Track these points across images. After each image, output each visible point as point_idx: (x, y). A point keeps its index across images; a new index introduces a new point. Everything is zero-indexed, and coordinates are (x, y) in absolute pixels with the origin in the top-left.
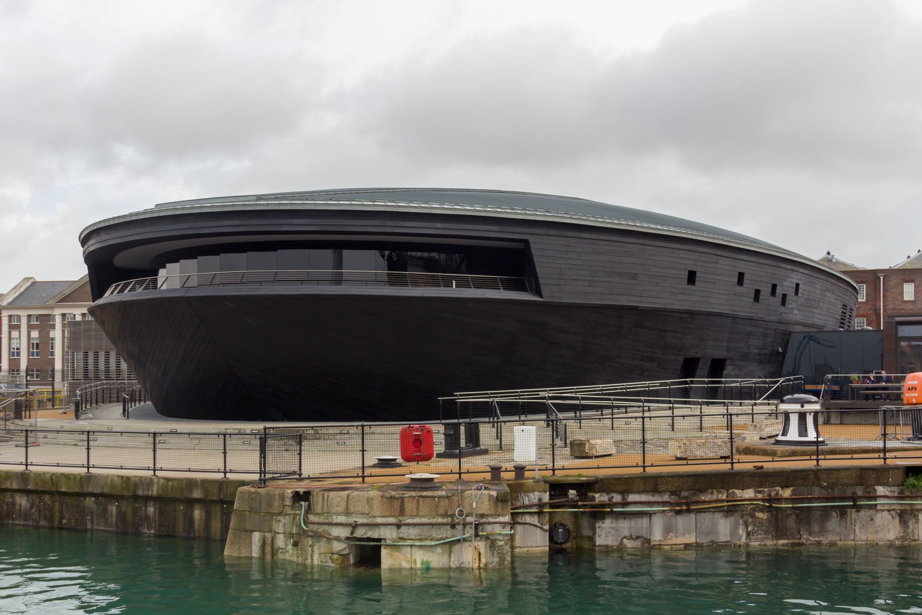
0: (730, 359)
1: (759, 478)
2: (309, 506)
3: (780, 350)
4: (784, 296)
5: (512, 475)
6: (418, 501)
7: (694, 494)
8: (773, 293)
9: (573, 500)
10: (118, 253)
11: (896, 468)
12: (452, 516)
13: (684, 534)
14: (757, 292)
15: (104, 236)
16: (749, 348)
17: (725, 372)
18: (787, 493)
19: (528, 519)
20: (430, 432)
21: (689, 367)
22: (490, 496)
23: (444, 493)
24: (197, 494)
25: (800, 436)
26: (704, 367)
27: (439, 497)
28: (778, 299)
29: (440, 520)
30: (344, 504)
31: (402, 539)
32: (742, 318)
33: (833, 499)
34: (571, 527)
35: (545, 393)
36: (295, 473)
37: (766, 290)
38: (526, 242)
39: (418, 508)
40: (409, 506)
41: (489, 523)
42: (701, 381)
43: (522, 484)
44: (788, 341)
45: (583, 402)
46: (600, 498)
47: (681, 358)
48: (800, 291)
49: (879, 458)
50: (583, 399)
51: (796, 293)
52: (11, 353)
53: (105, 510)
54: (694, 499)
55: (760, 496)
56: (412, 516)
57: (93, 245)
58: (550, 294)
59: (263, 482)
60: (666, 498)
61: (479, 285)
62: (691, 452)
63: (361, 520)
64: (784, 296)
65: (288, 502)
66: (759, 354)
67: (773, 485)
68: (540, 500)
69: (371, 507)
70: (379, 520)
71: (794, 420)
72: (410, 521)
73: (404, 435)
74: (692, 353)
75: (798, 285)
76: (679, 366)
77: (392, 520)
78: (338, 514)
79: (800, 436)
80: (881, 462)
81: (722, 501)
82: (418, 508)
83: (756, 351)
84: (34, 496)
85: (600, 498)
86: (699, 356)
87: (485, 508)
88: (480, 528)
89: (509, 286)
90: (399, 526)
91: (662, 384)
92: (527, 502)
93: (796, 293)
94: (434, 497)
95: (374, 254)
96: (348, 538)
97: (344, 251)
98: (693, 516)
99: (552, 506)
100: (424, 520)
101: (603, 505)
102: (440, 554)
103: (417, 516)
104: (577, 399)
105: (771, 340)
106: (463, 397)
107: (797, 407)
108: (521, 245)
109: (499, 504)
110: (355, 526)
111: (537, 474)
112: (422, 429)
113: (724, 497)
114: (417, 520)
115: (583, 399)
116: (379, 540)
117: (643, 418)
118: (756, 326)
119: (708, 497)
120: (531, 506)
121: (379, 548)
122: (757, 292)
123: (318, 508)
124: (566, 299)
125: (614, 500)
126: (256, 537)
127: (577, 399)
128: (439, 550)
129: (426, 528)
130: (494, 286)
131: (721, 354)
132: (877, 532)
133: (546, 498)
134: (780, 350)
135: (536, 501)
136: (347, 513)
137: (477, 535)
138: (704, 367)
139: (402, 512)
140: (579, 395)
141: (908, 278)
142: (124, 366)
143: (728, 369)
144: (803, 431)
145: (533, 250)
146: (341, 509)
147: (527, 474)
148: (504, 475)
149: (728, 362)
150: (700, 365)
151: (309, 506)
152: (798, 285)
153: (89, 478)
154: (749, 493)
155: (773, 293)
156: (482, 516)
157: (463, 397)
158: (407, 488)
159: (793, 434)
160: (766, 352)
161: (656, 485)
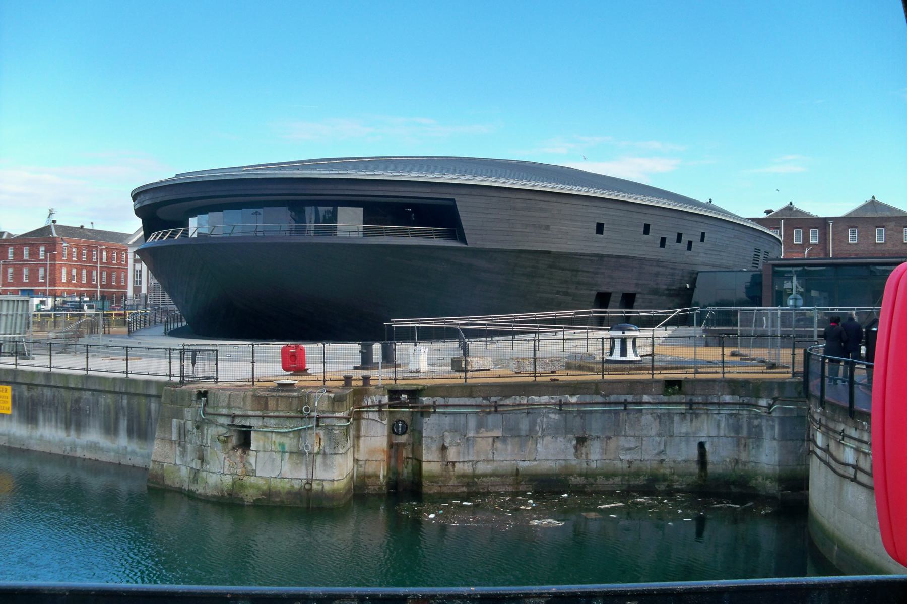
0: (640, 293)
1: (555, 387)
2: (207, 401)
3: (688, 286)
4: (690, 243)
5: (360, 383)
6: (277, 400)
7: (501, 400)
8: (679, 240)
9: (404, 402)
10: (162, 206)
11: (657, 381)
12: (301, 411)
13: (493, 430)
14: (663, 240)
15: (148, 197)
16: (657, 284)
17: (635, 304)
18: (574, 400)
19: (371, 415)
20: (302, 350)
21: (603, 300)
22: (329, 397)
23: (296, 394)
24: (153, 391)
25: (621, 356)
26: (616, 298)
27: (293, 397)
28: (684, 245)
29: (293, 414)
30: (227, 400)
31: (266, 427)
32: (650, 260)
33: (609, 404)
34: (408, 421)
35: (458, 322)
36: (213, 378)
37: (671, 238)
38: (454, 200)
39: (277, 405)
40: (271, 404)
41: (328, 417)
42: (613, 311)
43: (366, 390)
44: (696, 278)
45: (489, 328)
46: (425, 400)
47: (594, 293)
48: (706, 239)
49: (788, 373)
50: (489, 325)
51: (702, 240)
52: (135, 282)
53: (98, 401)
54: (502, 403)
55: (553, 401)
56: (273, 411)
57: (147, 200)
58: (473, 240)
59: (182, 383)
60: (479, 401)
61: (415, 235)
62: (524, 367)
63: (238, 412)
64: (690, 243)
65: (194, 398)
66: (668, 289)
67: (563, 394)
68: (380, 401)
69: (245, 403)
70: (250, 413)
71: (618, 343)
72: (272, 414)
73: (284, 351)
74: (604, 289)
75: (703, 234)
76: (593, 299)
77: (259, 413)
78: (223, 407)
79: (621, 356)
80: (650, 377)
81: (523, 405)
82: (277, 405)
83: (665, 287)
84: (54, 389)
85: (425, 400)
86: (610, 290)
87: (325, 406)
88: (321, 420)
89: (440, 235)
90: (263, 417)
91: (576, 314)
92: (370, 403)
93: (702, 240)
94: (289, 397)
95: (285, 208)
96: (229, 425)
97: (339, 208)
98: (499, 416)
99: (390, 406)
100: (281, 414)
101: (429, 406)
102: (291, 439)
103: (277, 410)
104: (484, 325)
105: (678, 277)
106: (397, 323)
107: (619, 334)
108: (451, 203)
109: (336, 404)
110: (234, 417)
111: (380, 383)
112: (297, 347)
113: (525, 402)
114: (276, 414)
115: (489, 325)
116: (250, 427)
117: (653, 337)
118: (663, 267)
119: (508, 402)
120: (373, 406)
121: (250, 432)
122: (663, 240)
123: (211, 402)
124: (488, 245)
125: (437, 403)
126: (175, 421)
127: (484, 325)
128: (291, 435)
129: (282, 420)
130: (427, 235)
131: (630, 289)
132: (642, 430)
133: (386, 400)
134: (688, 286)
135: (377, 403)
136: (229, 406)
137: (318, 426)
138: (616, 298)
139: (266, 407)
140: (486, 323)
141: (852, 225)
142: (167, 296)
143: (639, 300)
144: (624, 352)
145: (458, 208)
146: (225, 404)
147: (372, 383)
148: (354, 383)
149: (638, 296)
150: (612, 298)
151: (207, 401)
152: (703, 234)
153: (87, 377)
154: (545, 399)
155: (679, 240)
156: (323, 412)
157: (397, 323)
158: (273, 390)
159: (616, 356)
160: (674, 287)
161: (471, 392)
